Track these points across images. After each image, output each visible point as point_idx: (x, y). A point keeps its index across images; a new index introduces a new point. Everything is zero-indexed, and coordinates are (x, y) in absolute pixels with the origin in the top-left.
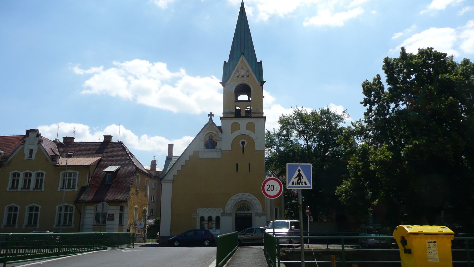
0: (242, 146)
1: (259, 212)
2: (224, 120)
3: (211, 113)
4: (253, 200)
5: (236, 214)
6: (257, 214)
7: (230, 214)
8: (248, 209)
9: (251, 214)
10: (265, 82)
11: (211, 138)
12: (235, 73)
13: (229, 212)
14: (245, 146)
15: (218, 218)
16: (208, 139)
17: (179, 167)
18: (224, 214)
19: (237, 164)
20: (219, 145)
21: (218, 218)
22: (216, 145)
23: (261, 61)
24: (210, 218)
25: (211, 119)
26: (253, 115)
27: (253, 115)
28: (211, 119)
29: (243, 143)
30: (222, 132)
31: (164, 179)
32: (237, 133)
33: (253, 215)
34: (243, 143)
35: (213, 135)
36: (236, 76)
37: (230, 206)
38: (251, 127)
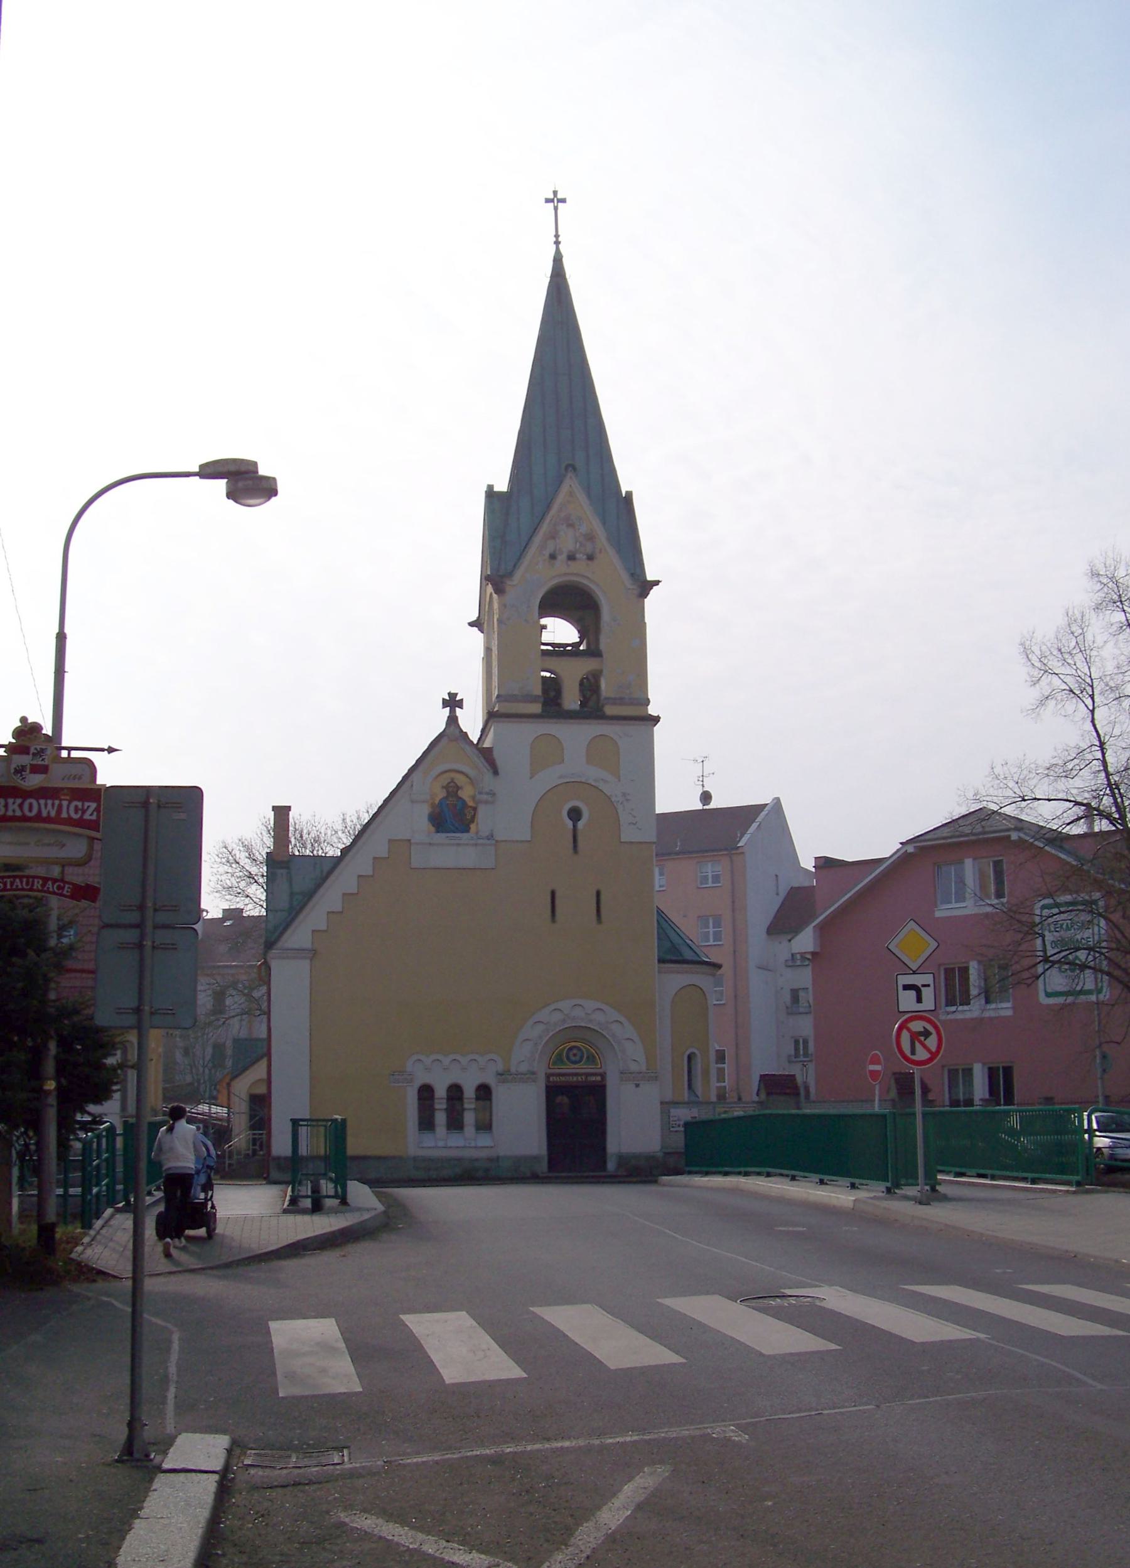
0: (570, 824)
1: (634, 1067)
3: (452, 696)
5: (548, 1076)
9: (603, 1076)
10: (657, 583)
11: (452, 790)
13: (523, 1068)
14: (580, 824)
15: (484, 1092)
16: (441, 794)
18: (504, 1076)
19: (553, 894)
21: (484, 1092)
25: (452, 720)
27: (609, 710)
28: (452, 720)
29: (575, 814)
30: (496, 772)
32: (549, 777)
34: (575, 814)
35: (460, 780)
37: (529, 1050)
38: (602, 754)
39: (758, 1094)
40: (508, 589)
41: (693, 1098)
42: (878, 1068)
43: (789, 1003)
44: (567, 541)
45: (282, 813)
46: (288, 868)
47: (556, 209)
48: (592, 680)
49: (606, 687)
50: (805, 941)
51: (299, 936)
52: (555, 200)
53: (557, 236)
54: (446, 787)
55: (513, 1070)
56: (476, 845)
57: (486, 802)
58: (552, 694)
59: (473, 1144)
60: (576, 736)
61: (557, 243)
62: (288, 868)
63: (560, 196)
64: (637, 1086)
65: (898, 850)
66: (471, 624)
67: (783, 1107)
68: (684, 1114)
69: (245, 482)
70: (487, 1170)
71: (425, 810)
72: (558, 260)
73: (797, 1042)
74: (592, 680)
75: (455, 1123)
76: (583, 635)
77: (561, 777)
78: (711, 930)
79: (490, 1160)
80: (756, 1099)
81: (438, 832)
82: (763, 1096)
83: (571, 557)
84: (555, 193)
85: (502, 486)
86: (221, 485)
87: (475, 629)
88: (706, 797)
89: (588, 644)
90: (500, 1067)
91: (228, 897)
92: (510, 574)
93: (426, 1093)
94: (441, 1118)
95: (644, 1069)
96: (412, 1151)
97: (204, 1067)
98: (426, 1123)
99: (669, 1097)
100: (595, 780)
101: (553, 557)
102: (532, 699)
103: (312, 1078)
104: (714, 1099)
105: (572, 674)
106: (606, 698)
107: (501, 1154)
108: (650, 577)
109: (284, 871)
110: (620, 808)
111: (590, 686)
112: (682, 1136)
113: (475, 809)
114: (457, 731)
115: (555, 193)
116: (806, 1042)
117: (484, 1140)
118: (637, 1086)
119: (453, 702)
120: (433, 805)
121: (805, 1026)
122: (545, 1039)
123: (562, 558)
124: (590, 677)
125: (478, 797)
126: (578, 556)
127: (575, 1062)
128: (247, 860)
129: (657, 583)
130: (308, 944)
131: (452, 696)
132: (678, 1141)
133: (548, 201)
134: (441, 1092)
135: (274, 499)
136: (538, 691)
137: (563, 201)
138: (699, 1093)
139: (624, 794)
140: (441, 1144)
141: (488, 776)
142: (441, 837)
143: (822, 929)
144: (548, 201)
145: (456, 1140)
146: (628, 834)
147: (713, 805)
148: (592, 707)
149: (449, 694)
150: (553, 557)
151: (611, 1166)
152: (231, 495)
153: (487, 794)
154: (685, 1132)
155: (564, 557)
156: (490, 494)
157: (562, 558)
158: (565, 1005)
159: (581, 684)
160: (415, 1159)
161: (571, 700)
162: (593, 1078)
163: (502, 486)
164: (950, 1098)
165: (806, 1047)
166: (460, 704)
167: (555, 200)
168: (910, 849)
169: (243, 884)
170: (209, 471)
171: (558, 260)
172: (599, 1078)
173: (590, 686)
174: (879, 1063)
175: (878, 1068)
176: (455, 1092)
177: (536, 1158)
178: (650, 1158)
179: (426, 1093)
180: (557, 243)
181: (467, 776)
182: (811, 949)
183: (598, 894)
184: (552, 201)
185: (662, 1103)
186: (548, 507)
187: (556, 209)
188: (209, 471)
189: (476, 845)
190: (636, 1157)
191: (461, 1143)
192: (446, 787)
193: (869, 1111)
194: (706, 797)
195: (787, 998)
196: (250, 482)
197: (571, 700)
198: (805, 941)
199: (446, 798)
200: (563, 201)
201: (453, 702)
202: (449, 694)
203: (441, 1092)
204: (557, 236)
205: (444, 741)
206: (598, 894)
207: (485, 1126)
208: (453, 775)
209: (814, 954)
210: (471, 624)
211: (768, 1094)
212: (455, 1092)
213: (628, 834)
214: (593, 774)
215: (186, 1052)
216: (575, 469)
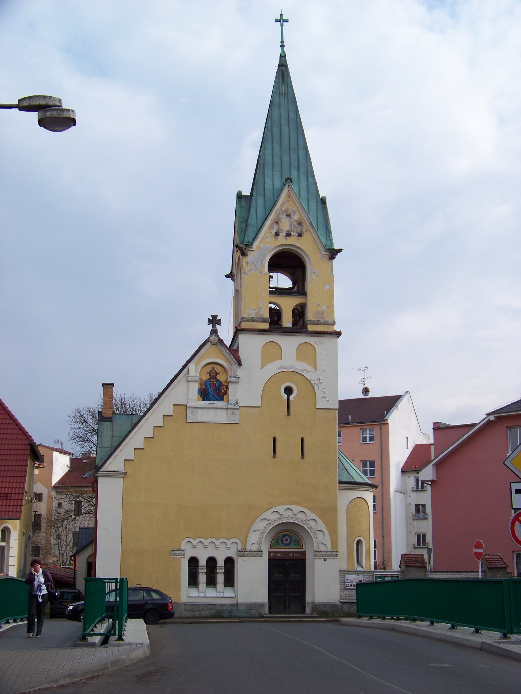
0: (285, 397)
1: (323, 548)
2: (105, 386)
3: (214, 317)
4: (319, 534)
5: (269, 553)
6: (318, 554)
7: (258, 553)
8: (299, 543)
9: (304, 553)
10: (340, 250)
11: (213, 375)
12: (271, 227)
13: (254, 548)
14: (292, 397)
15: (230, 562)
16: (206, 377)
17: (42, 615)
18: (242, 553)
19: (274, 439)
20: (235, 393)
21: (230, 562)
22: (226, 393)
23: (220, 320)
24: (211, 582)
25: (214, 332)
26: (310, 328)
27: (310, 328)
28: (214, 332)
29: (288, 391)
30: (240, 364)
31: (105, 468)
32: (273, 368)
33: (309, 557)
34: (288, 391)
35: (218, 369)
36: (274, 232)
37: (258, 538)
38: (307, 354)
39: (400, 567)
40: (249, 253)
41: (359, 568)
42: (477, 550)
43: (414, 513)
44: (285, 225)
45: (108, 387)
46: (112, 422)
47: (282, 26)
48: (300, 310)
49: (310, 315)
50: (428, 473)
51: (115, 464)
52: (281, 20)
53: (282, 42)
54: (209, 373)
55: (248, 549)
56: (227, 409)
57: (234, 383)
58: (276, 319)
59: (222, 595)
60: (289, 344)
61: (282, 46)
62: (112, 422)
63: (284, 18)
64: (325, 560)
65: (484, 419)
66: (227, 276)
67: (415, 574)
68: (353, 579)
69: (54, 116)
70: (230, 612)
71: (195, 388)
72: (283, 57)
73: (419, 536)
74: (300, 310)
75: (211, 582)
76: (294, 283)
77: (280, 368)
78: (368, 469)
79: (232, 605)
80: (399, 569)
81: (204, 400)
82: (403, 567)
83: (288, 235)
84: (281, 15)
85: (247, 192)
86: (34, 116)
87: (230, 279)
88: (366, 391)
89: (298, 289)
90: (240, 548)
91: (80, 443)
92: (249, 245)
93: (193, 562)
94: (202, 578)
95: (329, 549)
96: (184, 599)
97: (66, 546)
98: (193, 581)
99: (345, 568)
100: (301, 370)
101: (277, 234)
102: (264, 321)
103: (122, 552)
104: (373, 569)
105: (287, 305)
106: (310, 320)
107: (240, 601)
108: (336, 247)
109: (109, 423)
110: (316, 387)
111: (299, 313)
112: (354, 593)
113: (227, 387)
114: (217, 339)
115: (281, 15)
116: (424, 536)
117: (229, 593)
118: (325, 560)
119: (214, 321)
120: (201, 384)
121: (426, 527)
122: (268, 530)
123: (283, 234)
124: (299, 308)
125: (229, 379)
126: (292, 234)
127: (287, 545)
128: (92, 421)
129: (340, 250)
130: (121, 468)
131: (214, 317)
132: (352, 596)
133: (277, 21)
134: (203, 562)
135: (73, 127)
136: (267, 315)
137: (287, 21)
138: (364, 566)
139: (319, 379)
140: (202, 595)
141: (235, 366)
142: (206, 403)
143: (438, 465)
144: (277, 21)
145: (211, 592)
146: (321, 404)
147: (370, 396)
148: (300, 323)
149: (212, 316)
150: (277, 234)
151: (308, 610)
152: (41, 122)
153: (235, 377)
154: (357, 589)
155: (284, 234)
156: (240, 196)
157: (283, 234)
158: (281, 509)
159: (294, 310)
160: (185, 604)
161: (287, 321)
162: (298, 555)
163: (247, 192)
164: (517, 571)
165: (424, 540)
166: (219, 322)
167: (281, 20)
168: (492, 418)
169: (89, 435)
170: (26, 105)
171: (283, 57)
172: (301, 555)
173: (299, 313)
174: (481, 547)
175: (477, 550)
176: (212, 561)
177: (262, 605)
178: (333, 606)
179: (193, 562)
180: (282, 46)
181: (222, 366)
182: (431, 478)
183: (302, 440)
184: (280, 21)
185: (340, 571)
186: (275, 204)
187: (282, 26)
188: (26, 105)
189: (227, 409)
190: (325, 605)
191: (196, 594)
192: (209, 373)
193: (476, 577)
194: (366, 391)
195: (413, 509)
196: (55, 112)
197: (287, 321)
198: (428, 473)
199: (209, 379)
200: (287, 21)
201: (214, 321)
202: (212, 316)
203: (203, 562)
204: (282, 42)
205: (209, 344)
206: (302, 440)
207: (229, 581)
208: (213, 366)
209: (432, 481)
210: (227, 276)
211: (406, 566)
212: (212, 561)
213: (321, 404)
214: (300, 366)
215: (59, 537)
216: (291, 181)
